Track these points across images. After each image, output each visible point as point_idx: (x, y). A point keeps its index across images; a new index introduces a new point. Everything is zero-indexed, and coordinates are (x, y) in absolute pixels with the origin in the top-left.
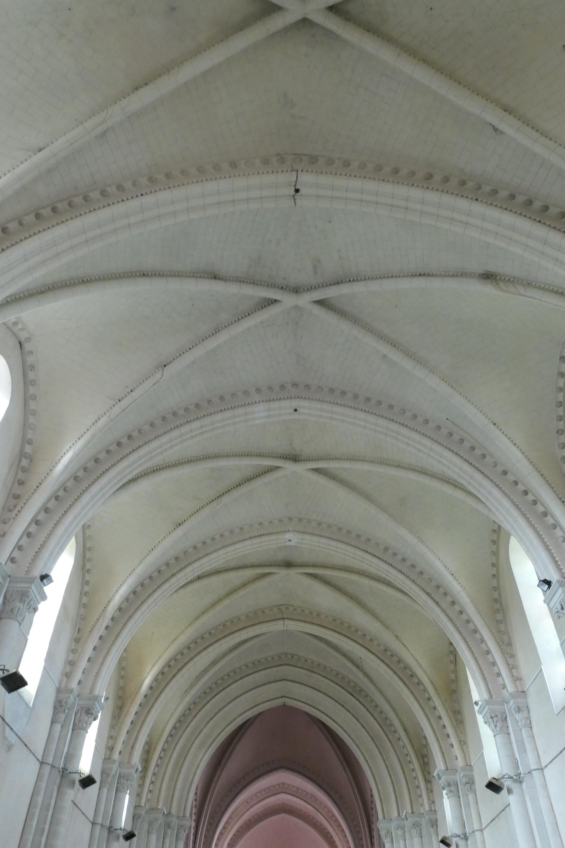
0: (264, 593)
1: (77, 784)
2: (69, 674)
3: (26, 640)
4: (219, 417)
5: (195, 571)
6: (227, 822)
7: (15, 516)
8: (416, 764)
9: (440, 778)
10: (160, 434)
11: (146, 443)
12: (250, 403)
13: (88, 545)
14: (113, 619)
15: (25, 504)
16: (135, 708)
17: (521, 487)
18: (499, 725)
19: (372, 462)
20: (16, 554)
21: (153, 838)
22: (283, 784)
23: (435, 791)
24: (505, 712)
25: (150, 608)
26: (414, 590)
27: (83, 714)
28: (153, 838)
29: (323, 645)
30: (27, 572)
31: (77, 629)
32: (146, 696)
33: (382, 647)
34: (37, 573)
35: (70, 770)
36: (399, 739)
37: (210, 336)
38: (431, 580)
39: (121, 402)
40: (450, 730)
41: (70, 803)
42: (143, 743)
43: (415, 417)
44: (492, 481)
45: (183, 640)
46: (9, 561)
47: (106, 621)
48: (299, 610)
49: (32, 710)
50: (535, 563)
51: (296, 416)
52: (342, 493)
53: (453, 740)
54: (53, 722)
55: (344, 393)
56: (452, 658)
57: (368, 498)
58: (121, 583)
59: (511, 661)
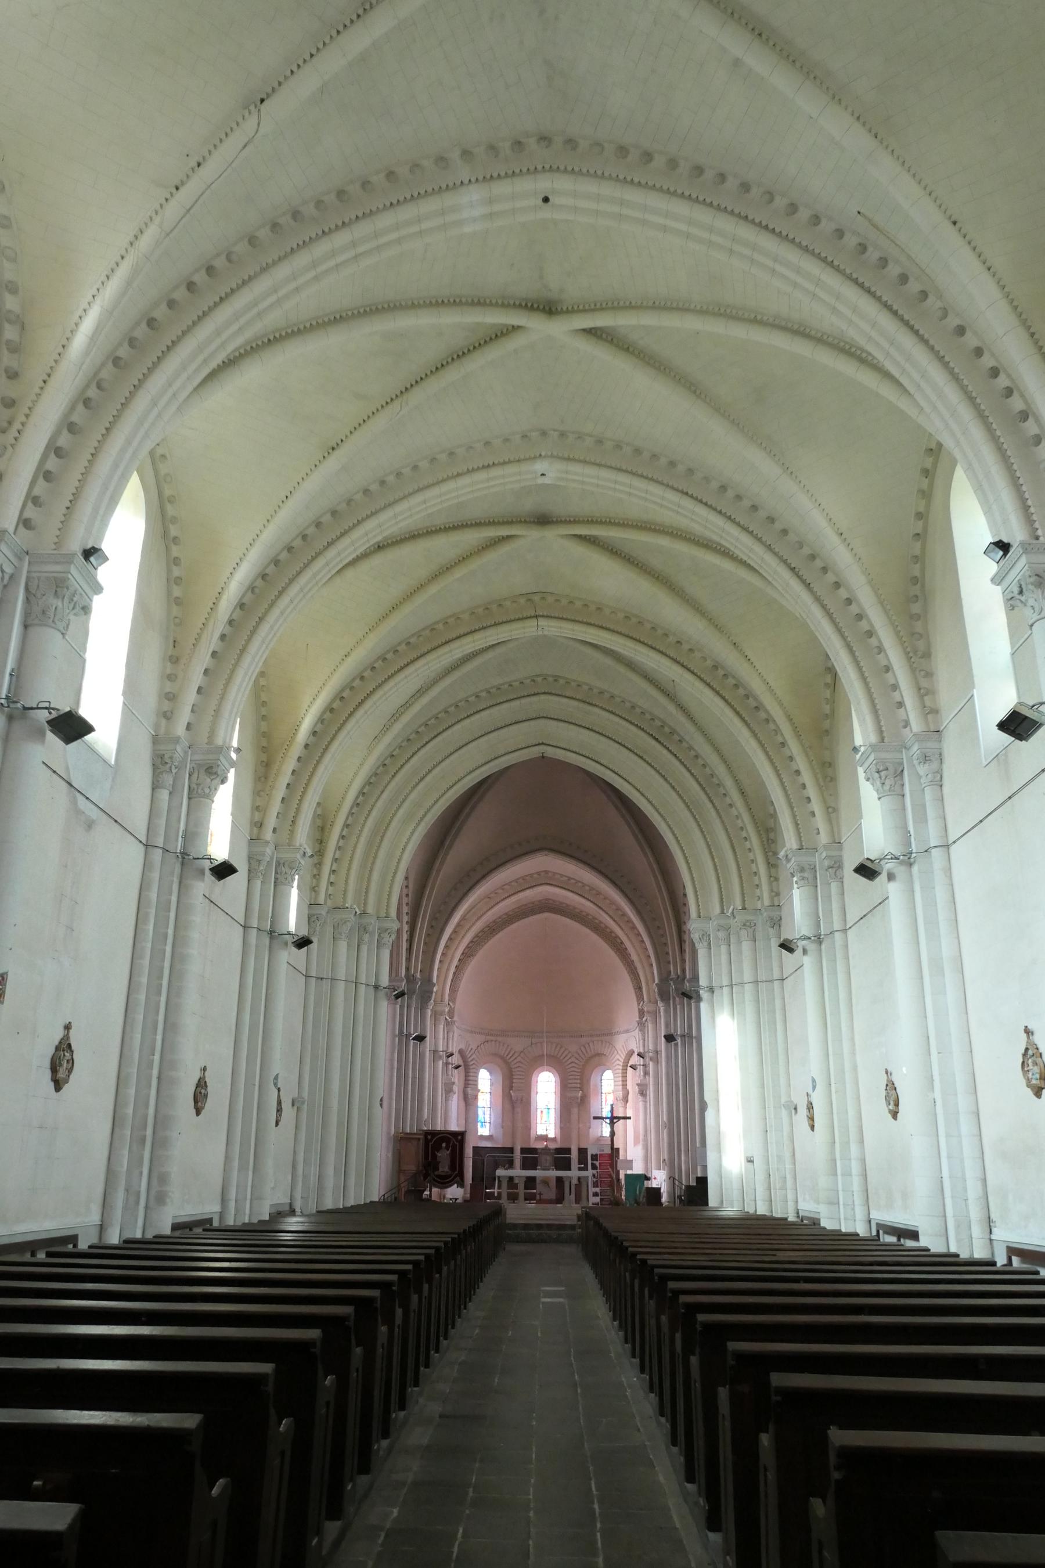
0: (504, 573)
1: (208, 873)
2: (169, 714)
3: (84, 661)
4: (386, 220)
5: (370, 536)
6: (459, 925)
7: (13, 441)
8: (755, 841)
9: (788, 860)
10: (270, 261)
11: (244, 283)
12: (451, 185)
13: (168, 492)
14: (231, 622)
15: (27, 416)
16: (290, 764)
17: (987, 361)
18: (888, 782)
19: (703, 312)
20: (31, 512)
21: (343, 945)
22: (546, 872)
23: (781, 878)
24: (902, 764)
25: (295, 602)
26: (768, 563)
27: (203, 775)
28: (343, 945)
29: (608, 661)
30: (58, 545)
31: (171, 642)
32: (306, 746)
33: (709, 662)
34: (75, 545)
35: (193, 854)
36: (731, 805)
37: (352, 21)
38: (801, 545)
39: (182, 190)
40: (812, 791)
41: (201, 898)
42: (310, 816)
43: (793, 208)
44: (932, 348)
45: (360, 655)
46: (21, 526)
47: (219, 625)
48: (564, 602)
49: (116, 770)
50: (988, 512)
51: (546, 213)
52: (642, 382)
53: (816, 806)
54: (155, 787)
55: (647, 157)
56: (829, 679)
57: (693, 388)
58: (238, 561)
59: (924, 683)
